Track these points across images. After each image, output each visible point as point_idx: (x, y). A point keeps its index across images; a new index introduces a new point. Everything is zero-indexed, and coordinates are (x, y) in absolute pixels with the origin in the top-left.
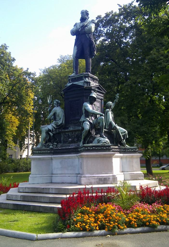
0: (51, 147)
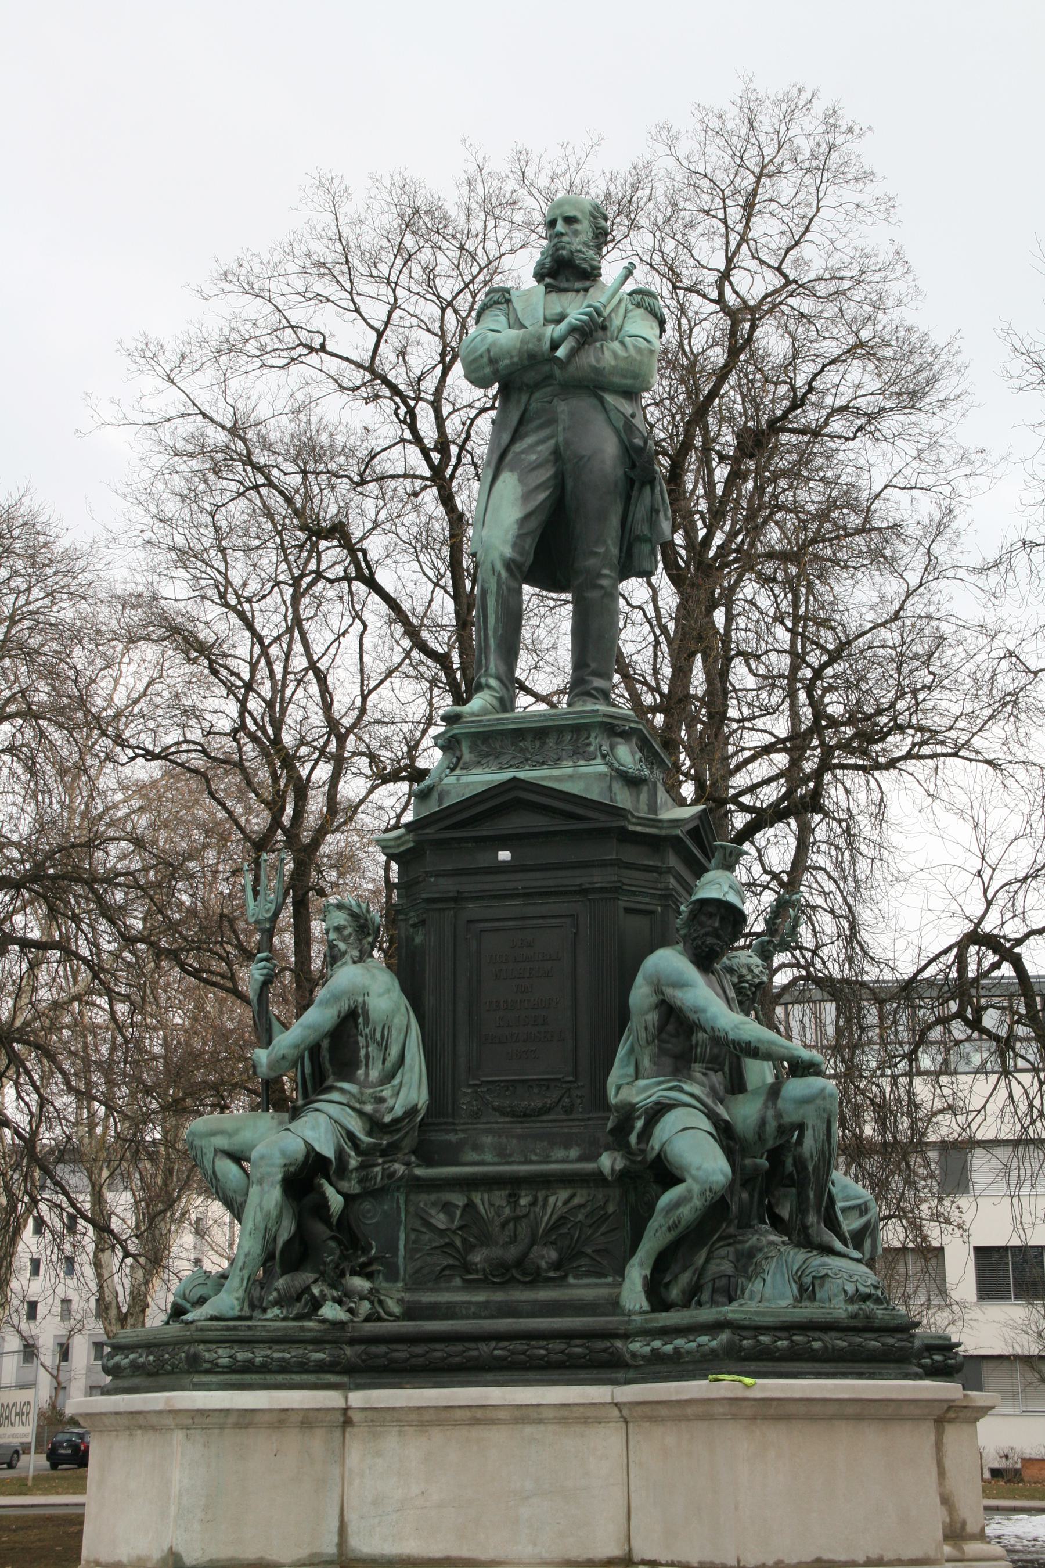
0: (330, 1311)
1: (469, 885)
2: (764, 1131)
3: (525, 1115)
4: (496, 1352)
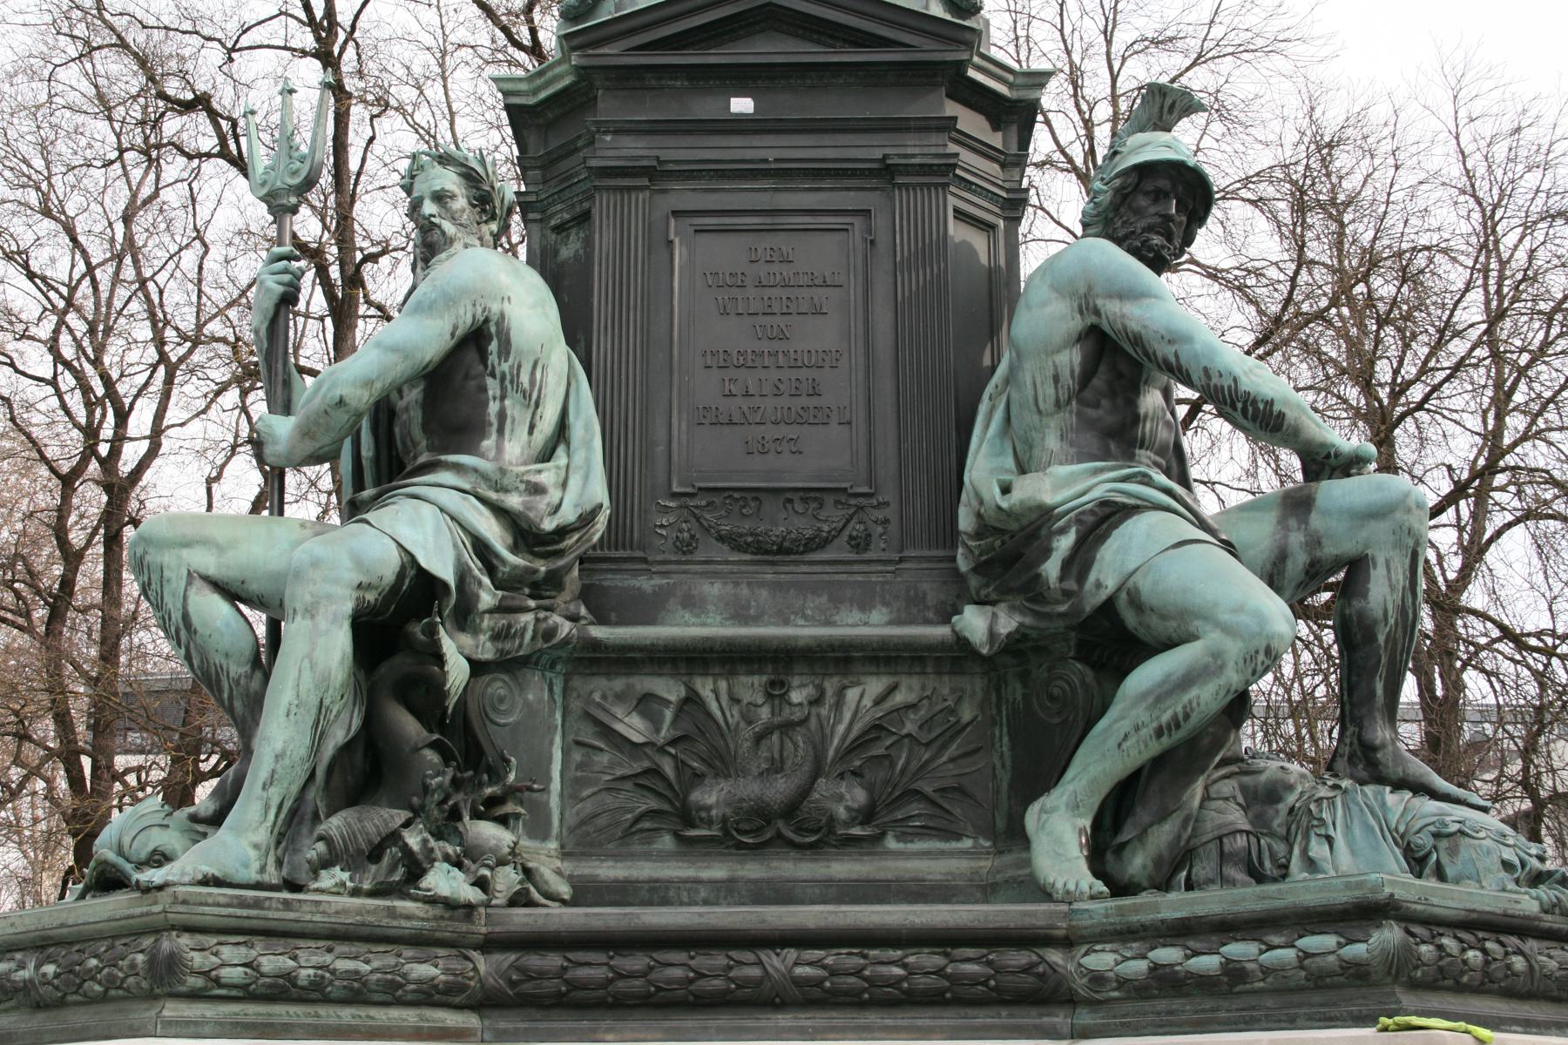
0: (444, 881)
1: (678, 150)
3: (781, 550)
4: (799, 971)
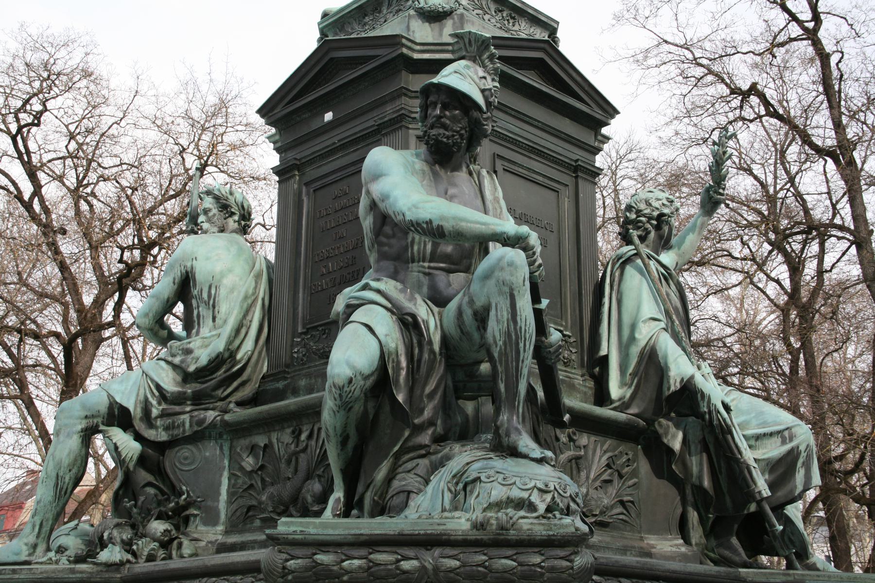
2: (463, 322)
